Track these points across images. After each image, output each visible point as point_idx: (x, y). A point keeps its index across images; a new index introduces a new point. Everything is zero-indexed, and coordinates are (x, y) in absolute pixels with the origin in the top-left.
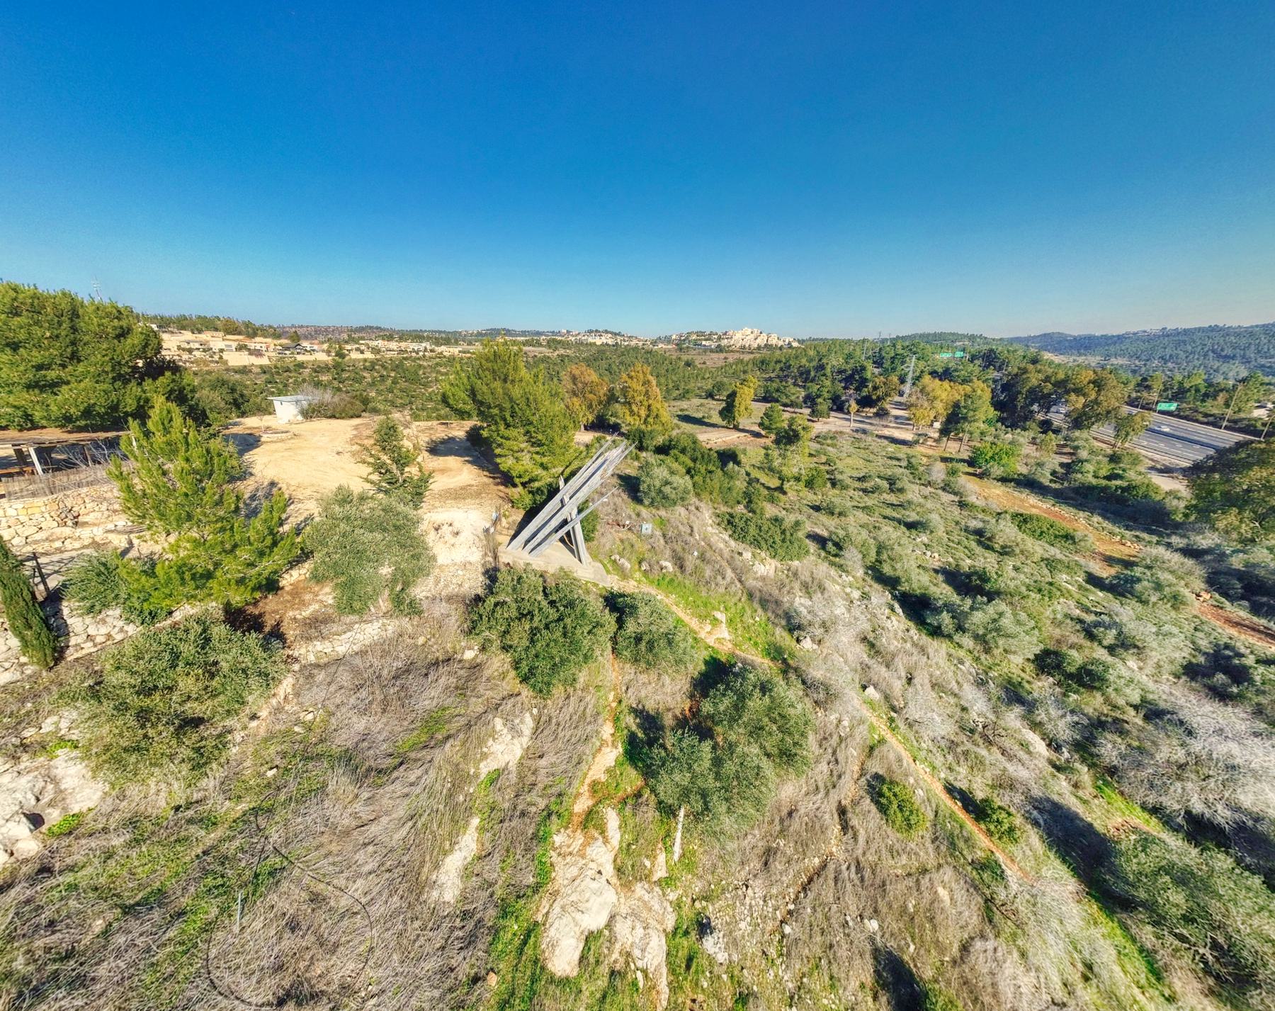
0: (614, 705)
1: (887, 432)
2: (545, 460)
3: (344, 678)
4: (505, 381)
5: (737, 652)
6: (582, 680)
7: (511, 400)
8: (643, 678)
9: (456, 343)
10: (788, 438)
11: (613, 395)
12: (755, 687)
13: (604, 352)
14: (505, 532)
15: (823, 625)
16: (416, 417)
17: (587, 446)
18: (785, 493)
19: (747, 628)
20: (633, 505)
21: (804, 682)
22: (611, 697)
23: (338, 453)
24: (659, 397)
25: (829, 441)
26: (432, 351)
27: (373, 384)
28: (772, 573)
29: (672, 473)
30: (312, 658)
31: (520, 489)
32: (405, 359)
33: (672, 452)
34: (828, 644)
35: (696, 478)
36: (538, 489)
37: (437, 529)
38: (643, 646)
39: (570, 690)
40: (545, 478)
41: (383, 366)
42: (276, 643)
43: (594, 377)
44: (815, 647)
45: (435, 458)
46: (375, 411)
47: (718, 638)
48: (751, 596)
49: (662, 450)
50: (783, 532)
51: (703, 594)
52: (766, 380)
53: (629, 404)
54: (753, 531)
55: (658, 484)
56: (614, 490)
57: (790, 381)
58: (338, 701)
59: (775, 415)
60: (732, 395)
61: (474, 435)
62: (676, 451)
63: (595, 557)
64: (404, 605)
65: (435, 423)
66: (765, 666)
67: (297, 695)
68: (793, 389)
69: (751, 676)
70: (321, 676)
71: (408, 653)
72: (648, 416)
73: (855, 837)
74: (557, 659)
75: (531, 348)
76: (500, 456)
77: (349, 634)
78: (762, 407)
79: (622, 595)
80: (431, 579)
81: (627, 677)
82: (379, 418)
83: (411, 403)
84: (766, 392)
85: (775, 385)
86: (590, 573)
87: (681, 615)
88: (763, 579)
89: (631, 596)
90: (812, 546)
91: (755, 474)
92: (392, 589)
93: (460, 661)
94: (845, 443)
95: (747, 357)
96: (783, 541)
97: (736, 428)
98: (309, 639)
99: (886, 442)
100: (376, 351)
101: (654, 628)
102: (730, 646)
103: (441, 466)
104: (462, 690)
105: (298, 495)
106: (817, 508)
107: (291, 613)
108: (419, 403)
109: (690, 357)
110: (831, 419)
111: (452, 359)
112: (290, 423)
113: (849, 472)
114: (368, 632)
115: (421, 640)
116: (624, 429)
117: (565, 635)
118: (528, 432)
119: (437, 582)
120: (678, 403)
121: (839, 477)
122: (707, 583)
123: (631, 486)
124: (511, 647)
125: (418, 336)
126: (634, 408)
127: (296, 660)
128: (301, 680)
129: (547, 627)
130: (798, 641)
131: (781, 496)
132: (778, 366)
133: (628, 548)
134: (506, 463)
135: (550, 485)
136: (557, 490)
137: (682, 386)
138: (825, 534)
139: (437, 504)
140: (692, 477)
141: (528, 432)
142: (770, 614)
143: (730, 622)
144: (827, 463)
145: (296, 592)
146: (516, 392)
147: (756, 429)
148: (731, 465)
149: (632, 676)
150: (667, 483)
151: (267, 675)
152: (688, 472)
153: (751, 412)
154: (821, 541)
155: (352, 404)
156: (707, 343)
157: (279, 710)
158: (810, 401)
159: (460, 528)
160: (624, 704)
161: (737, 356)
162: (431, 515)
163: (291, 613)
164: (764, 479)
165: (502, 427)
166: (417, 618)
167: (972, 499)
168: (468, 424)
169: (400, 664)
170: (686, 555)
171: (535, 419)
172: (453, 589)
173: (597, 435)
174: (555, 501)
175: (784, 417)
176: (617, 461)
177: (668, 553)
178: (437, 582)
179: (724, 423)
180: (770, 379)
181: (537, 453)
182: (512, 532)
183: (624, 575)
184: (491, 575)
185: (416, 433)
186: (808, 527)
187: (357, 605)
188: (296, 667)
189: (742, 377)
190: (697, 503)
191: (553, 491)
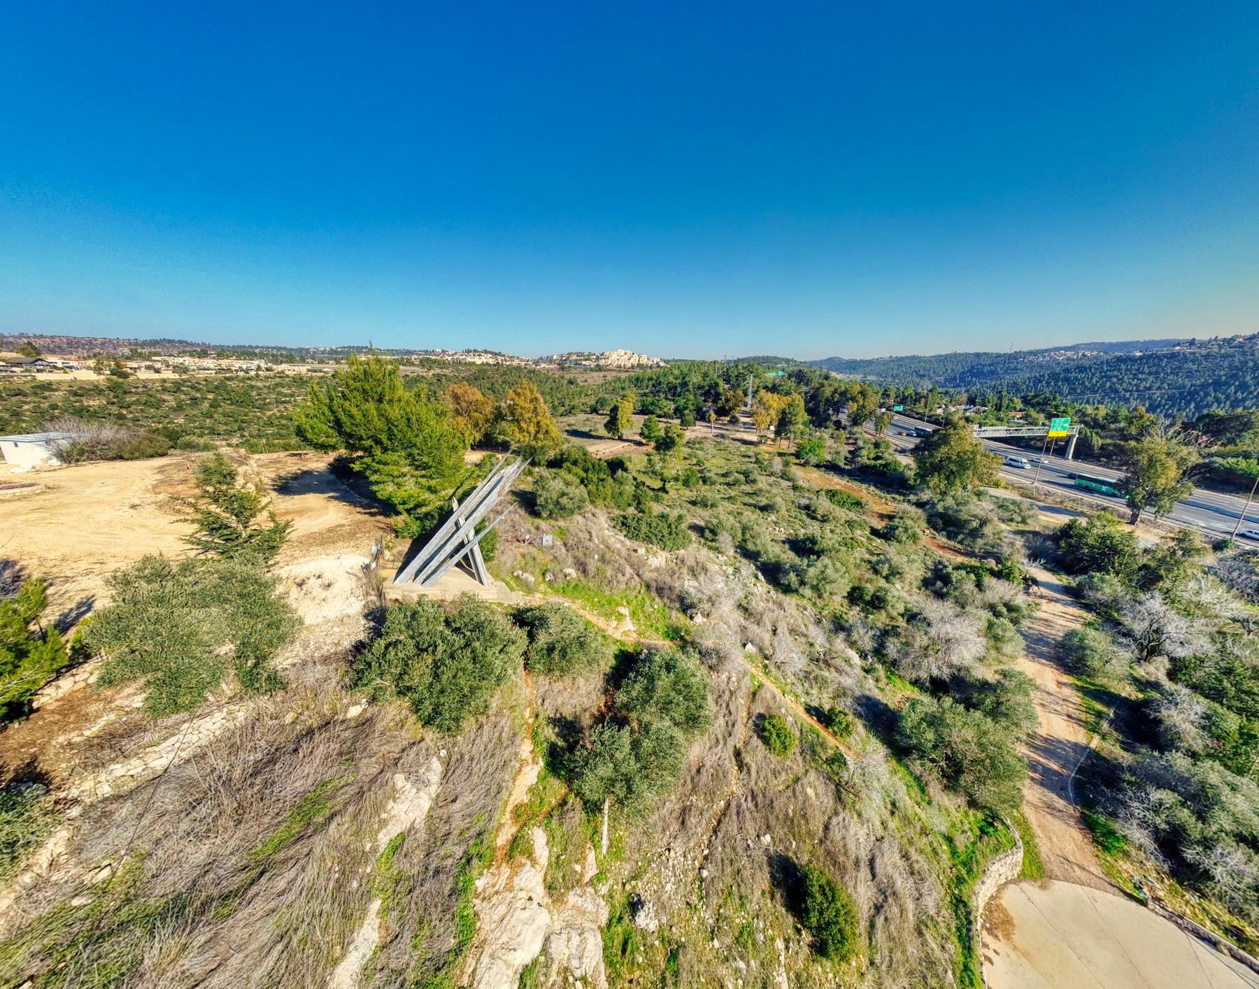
1: (739, 435)
2: (433, 483)
4: (380, 400)
6: (494, 705)
7: (388, 420)
8: (558, 686)
9: (303, 360)
10: (665, 444)
11: (500, 413)
13: (485, 371)
16: (253, 449)
18: (667, 492)
19: (648, 617)
20: (530, 519)
21: (700, 653)
22: (527, 713)
23: (133, 507)
24: (548, 414)
26: (268, 370)
27: (179, 408)
28: (663, 564)
29: (567, 484)
31: (404, 516)
32: (229, 379)
33: (565, 465)
35: (590, 487)
37: (300, 585)
38: (556, 655)
39: (482, 719)
40: (434, 502)
41: (193, 388)
45: (287, 497)
46: (190, 446)
47: (624, 630)
48: (648, 587)
49: (555, 464)
50: (669, 527)
53: (518, 421)
54: (644, 528)
55: (555, 497)
57: (662, 396)
60: (615, 410)
63: (496, 576)
65: (282, 454)
66: (666, 646)
68: (665, 403)
69: (657, 658)
72: (538, 432)
73: (749, 772)
74: (466, 690)
76: (377, 483)
77: (172, 740)
81: (542, 690)
86: (493, 593)
87: (589, 617)
88: (657, 570)
89: (539, 608)
90: (694, 536)
91: (641, 478)
93: (343, 722)
94: (709, 447)
95: (623, 375)
96: (670, 534)
97: (620, 439)
99: (739, 444)
101: (565, 635)
102: (635, 636)
106: (694, 503)
108: (254, 429)
109: (572, 376)
111: (300, 381)
113: (715, 470)
115: (289, 718)
118: (410, 455)
120: (565, 419)
121: (708, 475)
123: (528, 502)
125: (246, 352)
126: (523, 425)
130: (691, 618)
132: (650, 383)
133: (531, 563)
134: (386, 490)
135: (441, 508)
136: (451, 512)
137: (567, 402)
138: (702, 524)
139: (297, 554)
141: (410, 455)
142: (665, 600)
146: (395, 412)
147: (638, 438)
148: (620, 472)
150: (563, 494)
153: (632, 425)
154: (699, 530)
156: (587, 363)
158: (679, 412)
159: (329, 575)
161: (614, 374)
162: (289, 567)
165: (377, 451)
167: (800, 483)
168: (331, 457)
169: (259, 756)
171: (418, 441)
172: (327, 649)
175: (660, 428)
177: (570, 560)
179: (610, 435)
180: (645, 395)
181: (423, 476)
182: (400, 565)
183: (529, 589)
184: (377, 617)
185: (256, 470)
186: (690, 519)
189: (622, 393)
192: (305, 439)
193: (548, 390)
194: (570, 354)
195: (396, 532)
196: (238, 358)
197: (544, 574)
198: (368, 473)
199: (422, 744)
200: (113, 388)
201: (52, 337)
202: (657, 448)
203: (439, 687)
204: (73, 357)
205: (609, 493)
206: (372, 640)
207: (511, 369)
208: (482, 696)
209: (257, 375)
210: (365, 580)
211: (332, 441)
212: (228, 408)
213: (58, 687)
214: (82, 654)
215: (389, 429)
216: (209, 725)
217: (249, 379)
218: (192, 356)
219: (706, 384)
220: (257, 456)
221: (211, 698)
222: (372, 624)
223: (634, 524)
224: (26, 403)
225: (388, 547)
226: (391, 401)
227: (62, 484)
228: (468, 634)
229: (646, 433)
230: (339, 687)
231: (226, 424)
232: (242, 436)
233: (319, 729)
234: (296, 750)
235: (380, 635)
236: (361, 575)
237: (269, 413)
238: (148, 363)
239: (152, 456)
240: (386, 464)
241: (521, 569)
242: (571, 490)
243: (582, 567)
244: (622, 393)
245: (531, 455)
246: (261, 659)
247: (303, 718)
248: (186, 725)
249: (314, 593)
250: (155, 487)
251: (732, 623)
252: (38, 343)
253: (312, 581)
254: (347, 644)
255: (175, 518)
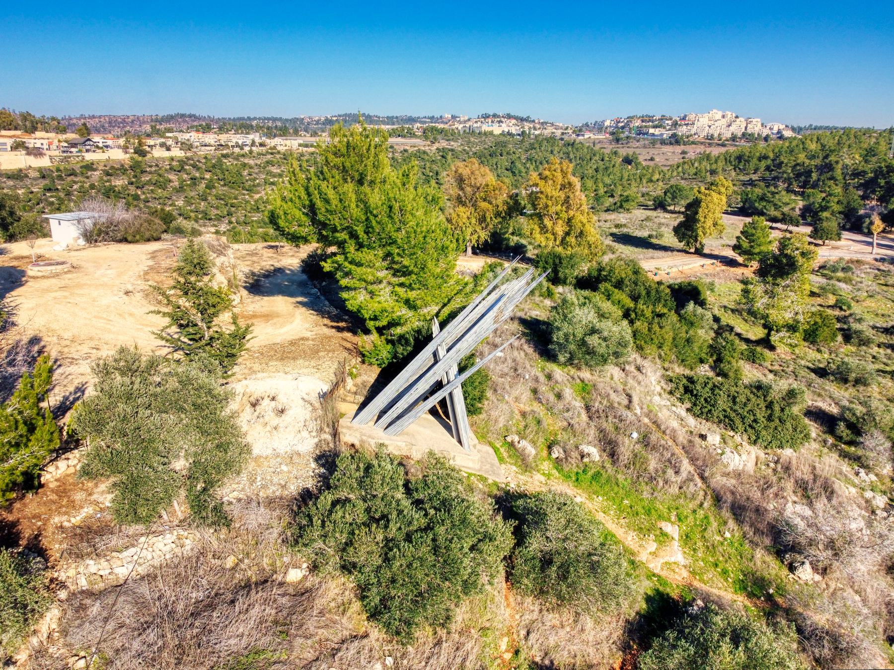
0: (508, 656)
2: (412, 295)
3: (126, 611)
4: (360, 182)
5: (696, 584)
6: (459, 618)
7: (367, 210)
8: (552, 618)
9: (296, 133)
10: (778, 267)
11: (517, 203)
12: (723, 635)
13: (504, 144)
14: (350, 398)
15: (831, 544)
16: (235, 237)
17: (475, 277)
18: (772, 348)
19: (711, 548)
20: (541, 362)
21: (800, 630)
22: (504, 644)
23: (127, 293)
24: (585, 208)
25: (840, 274)
26: (261, 145)
27: (180, 190)
28: (750, 467)
29: (602, 316)
30: (83, 583)
31: (374, 336)
32: (225, 156)
33: (602, 286)
34: (837, 574)
35: (638, 324)
36: (401, 337)
37: (254, 405)
38: (553, 571)
39: (442, 632)
40: (412, 322)
42: (36, 563)
43: (490, 178)
44: (818, 578)
45: (257, 298)
46: (179, 231)
47: (668, 561)
48: (718, 499)
49: (587, 283)
50: (770, 406)
51: (646, 495)
52: (744, 184)
53: (540, 217)
54: (723, 402)
56: (512, 340)
57: (782, 186)
58: (118, 644)
59: (759, 233)
60: (694, 205)
61: (311, 266)
62: (608, 285)
63: (482, 436)
64: (208, 511)
65: (260, 245)
66: (738, 604)
67: (64, 633)
68: (786, 197)
69: (718, 619)
70: (95, 609)
71: (213, 579)
72: (567, 234)
74: (424, 587)
75: (400, 140)
76: (347, 289)
77: (132, 551)
78: (739, 223)
79: (523, 496)
80: (244, 476)
81: (528, 617)
82: (183, 242)
83: (230, 214)
84: (745, 202)
85: (758, 191)
86: (475, 461)
87: (611, 526)
88: (738, 475)
89: (537, 497)
90: (814, 429)
91: (728, 319)
92: (190, 490)
93: (281, 584)
95: (716, 151)
96: (770, 418)
97: (699, 252)
98: (80, 556)
100: (187, 146)
101: (570, 545)
102: (685, 574)
103: (265, 310)
104: (284, 626)
105: (74, 351)
106: (822, 373)
107: (56, 520)
108: (240, 214)
109: (630, 152)
110: (842, 243)
111: (286, 156)
112: (69, 249)
113: (870, 320)
114: (158, 547)
115: (230, 562)
116: (531, 253)
117: (435, 550)
118: (389, 254)
119: (252, 481)
120: (612, 216)
121: (855, 326)
122: (652, 479)
123: (540, 336)
124: (354, 565)
125: (244, 125)
126: (548, 222)
127: (63, 585)
128: (70, 613)
129: (408, 538)
130: (792, 568)
131: (767, 353)
132: (763, 164)
133: (533, 426)
134: (356, 300)
135: (419, 332)
136: (429, 338)
137: (619, 191)
138: (834, 410)
139: (256, 367)
140: (632, 322)
141: (389, 254)
142: (746, 528)
143: (687, 538)
144: (838, 306)
145: (63, 490)
146: (375, 198)
147: (730, 253)
148: (691, 306)
149: (535, 615)
150: (593, 331)
151: (25, 606)
152: (626, 315)
153: (722, 230)
154: (828, 422)
155: (149, 222)
157: (40, 653)
158: (810, 215)
159: (286, 398)
160: (522, 655)
161: (700, 149)
162: (247, 382)
163: (56, 520)
164: (741, 327)
165: (351, 247)
166: (224, 530)
168: (306, 250)
169: (201, 595)
170: (620, 438)
171: (400, 236)
172: (273, 491)
173: (490, 260)
174: (426, 354)
175: (772, 238)
176: (519, 298)
177: (592, 432)
178: (252, 481)
179: (681, 245)
180: (751, 183)
181: (402, 285)
182: (361, 399)
183: (525, 465)
184: (328, 461)
185: (233, 261)
186: (809, 400)
187: (143, 512)
188: (63, 595)
189: (709, 179)
190: (639, 360)
191: (422, 340)
192: (278, 228)
193: (591, 172)
194: (630, 119)
195: (364, 355)
196: (236, 133)
197: (550, 447)
198: (339, 275)
199: (365, 641)
200: (136, 167)
201: (100, 117)
202: (762, 273)
203: (389, 574)
204: (110, 136)
205: (669, 337)
206: (320, 491)
207: (540, 141)
208: (444, 602)
209: (251, 152)
210: (320, 412)
211: (303, 231)
212: (220, 189)
213: (57, 468)
214: (71, 443)
215: (367, 219)
216: (160, 546)
217: (243, 156)
218: (198, 131)
219: (868, 167)
220: (236, 246)
221: (165, 517)
222: (323, 470)
223: (706, 393)
224: (75, 182)
225: (350, 374)
226: (372, 183)
227: (83, 264)
228: (432, 512)
229: (745, 246)
230: (280, 541)
231: (217, 208)
232: (230, 222)
233: (256, 584)
234: (233, 602)
235: (329, 487)
236: (317, 405)
237: (257, 196)
238: (163, 140)
239: (149, 240)
240: (359, 264)
241: (519, 433)
242: (607, 326)
243: (611, 449)
244: (709, 179)
245: (554, 270)
246: (210, 484)
247: (243, 566)
248: (143, 539)
249: (267, 418)
250: (146, 273)
251: (871, 596)
252: (91, 123)
253: (266, 402)
254: (294, 489)
255: (152, 308)
